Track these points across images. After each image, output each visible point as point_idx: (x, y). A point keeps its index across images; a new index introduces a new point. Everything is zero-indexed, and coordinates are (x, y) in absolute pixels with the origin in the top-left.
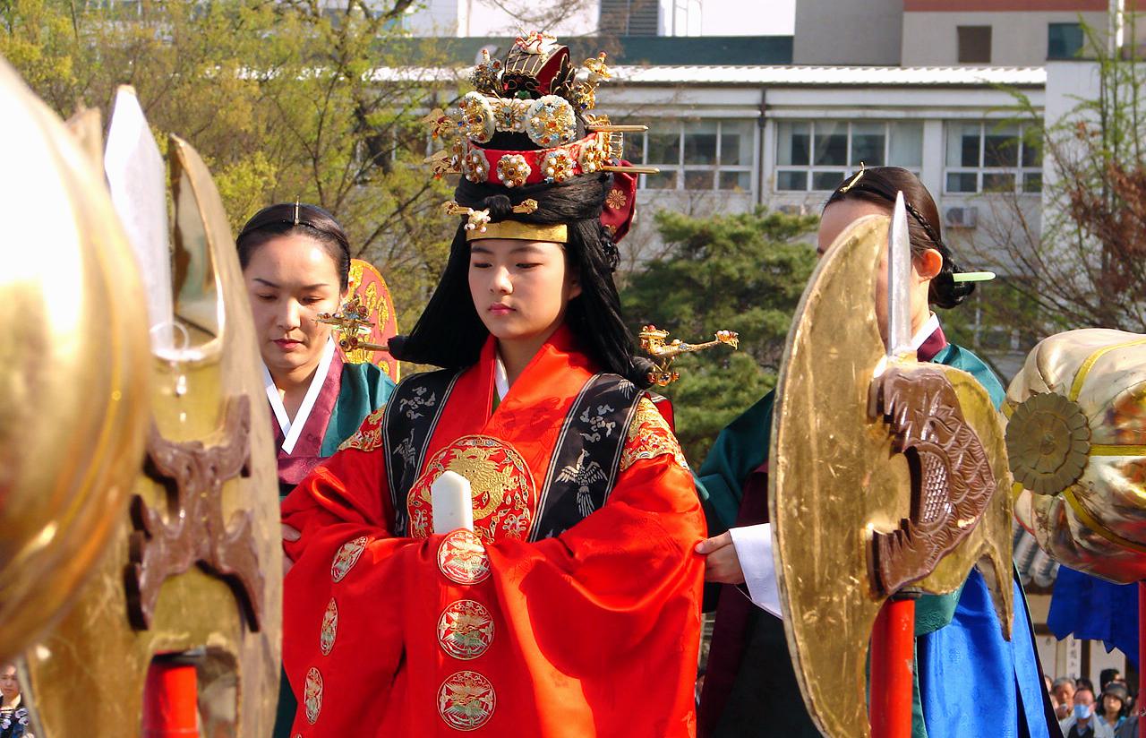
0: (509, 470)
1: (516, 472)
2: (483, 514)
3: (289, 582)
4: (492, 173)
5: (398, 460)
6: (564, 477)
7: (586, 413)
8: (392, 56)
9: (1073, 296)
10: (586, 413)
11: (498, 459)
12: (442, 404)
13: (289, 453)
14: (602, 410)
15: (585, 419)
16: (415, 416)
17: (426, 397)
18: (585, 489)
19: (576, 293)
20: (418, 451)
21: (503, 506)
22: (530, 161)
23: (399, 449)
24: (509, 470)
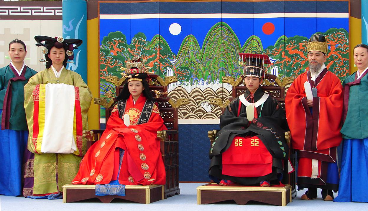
0: (137, 112)
1: (139, 112)
2: (134, 118)
3: (310, 74)
4: (132, 72)
5: (121, 112)
6: (144, 112)
7: (142, 119)
8: (123, 73)
9: (60, 191)
10: (142, 119)
11: (136, 111)
12: (126, 104)
13: (289, 172)
14: (144, 119)
15: (141, 120)
16: (122, 106)
17: (123, 103)
18: (147, 114)
19: (144, 89)
20: (124, 110)
21: (137, 117)
22: (137, 70)
23: (120, 111)
24: (137, 112)
